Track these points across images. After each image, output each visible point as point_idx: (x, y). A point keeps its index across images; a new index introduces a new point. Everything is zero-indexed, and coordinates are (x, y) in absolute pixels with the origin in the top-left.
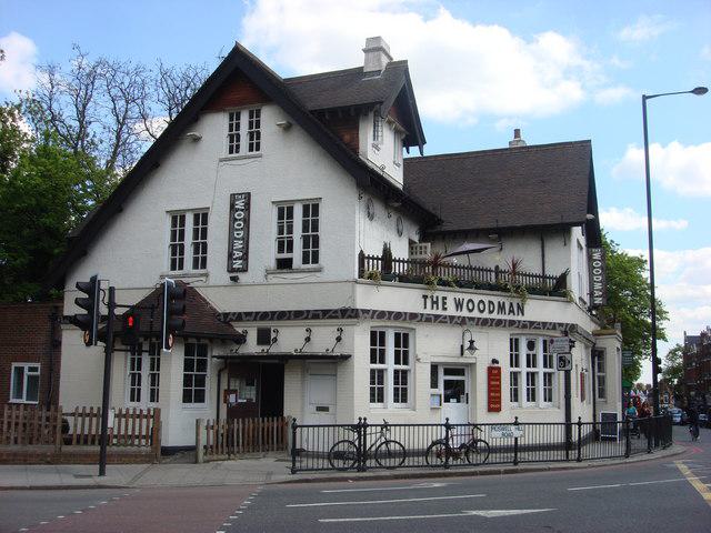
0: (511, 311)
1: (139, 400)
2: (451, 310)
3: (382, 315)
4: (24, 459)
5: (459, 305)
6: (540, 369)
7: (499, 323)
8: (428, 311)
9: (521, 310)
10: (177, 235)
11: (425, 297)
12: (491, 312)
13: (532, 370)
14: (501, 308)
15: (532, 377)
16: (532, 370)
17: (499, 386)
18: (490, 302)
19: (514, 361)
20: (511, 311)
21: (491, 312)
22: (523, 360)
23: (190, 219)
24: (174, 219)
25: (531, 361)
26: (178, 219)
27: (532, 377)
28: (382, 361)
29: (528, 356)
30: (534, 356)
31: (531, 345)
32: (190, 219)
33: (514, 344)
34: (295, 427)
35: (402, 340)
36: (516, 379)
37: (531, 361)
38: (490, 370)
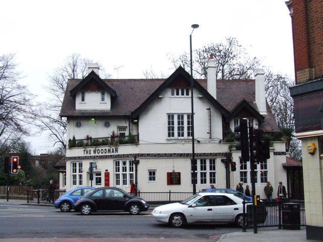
0: (113, 152)
1: (126, 184)
2: (92, 154)
3: (75, 158)
4: (217, 196)
5: (95, 152)
6: (128, 172)
7: (111, 156)
8: (85, 155)
9: (117, 151)
10: (171, 123)
11: (84, 151)
12: (105, 153)
13: (124, 173)
14: (109, 151)
15: (125, 176)
16: (124, 173)
17: (105, 181)
18: (105, 149)
19: (118, 170)
20: (113, 152)
21: (105, 153)
22: (78, 177)
23: (176, 118)
24: (169, 116)
25: (124, 169)
26: (170, 116)
27: (125, 176)
28: (126, 171)
29: (123, 167)
30: (126, 167)
31: (124, 163)
32: (176, 118)
33: (117, 164)
34: (139, 193)
35: (81, 165)
36: (80, 182)
37: (124, 169)
38: (93, 180)
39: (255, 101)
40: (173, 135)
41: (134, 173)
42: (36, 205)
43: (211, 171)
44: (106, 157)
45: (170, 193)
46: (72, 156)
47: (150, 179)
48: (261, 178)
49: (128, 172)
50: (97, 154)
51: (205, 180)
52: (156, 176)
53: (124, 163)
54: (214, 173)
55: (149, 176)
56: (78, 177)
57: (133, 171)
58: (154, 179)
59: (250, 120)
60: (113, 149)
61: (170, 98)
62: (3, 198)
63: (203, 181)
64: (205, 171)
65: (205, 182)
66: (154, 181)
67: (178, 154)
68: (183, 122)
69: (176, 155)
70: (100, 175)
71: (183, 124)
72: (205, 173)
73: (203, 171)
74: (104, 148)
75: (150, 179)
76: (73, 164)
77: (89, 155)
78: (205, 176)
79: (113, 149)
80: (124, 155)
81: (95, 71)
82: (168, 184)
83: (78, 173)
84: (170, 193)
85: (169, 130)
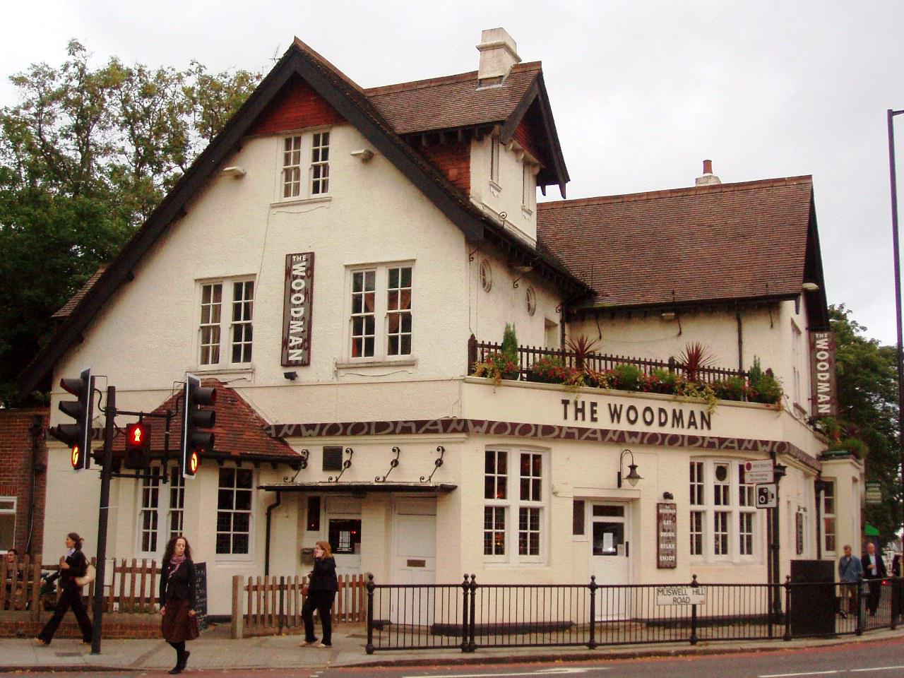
2: (604, 422)
5: (615, 414)
8: (571, 422)
9: (706, 420)
11: (566, 403)
12: (662, 424)
13: (722, 508)
15: (721, 519)
18: (661, 410)
19: (696, 495)
20: (692, 424)
21: (662, 424)
25: (721, 495)
27: (721, 519)
29: (717, 488)
30: (726, 488)
31: (721, 473)
33: (696, 471)
35: (531, 465)
37: (721, 495)
40: (370, 350)
44: (673, 441)
45: (593, 587)
46: (508, 420)
50: (624, 426)
53: (721, 473)
54: (535, 512)
60: (692, 413)
62: (16, 632)
65: (500, 551)
67: (323, 426)
68: (217, 310)
69: (637, 440)
71: (217, 318)
72: (501, 510)
74: (655, 406)
77: (587, 424)
79: (692, 413)
80: (741, 442)
83: (513, 502)
84: (593, 587)
85: (357, 330)
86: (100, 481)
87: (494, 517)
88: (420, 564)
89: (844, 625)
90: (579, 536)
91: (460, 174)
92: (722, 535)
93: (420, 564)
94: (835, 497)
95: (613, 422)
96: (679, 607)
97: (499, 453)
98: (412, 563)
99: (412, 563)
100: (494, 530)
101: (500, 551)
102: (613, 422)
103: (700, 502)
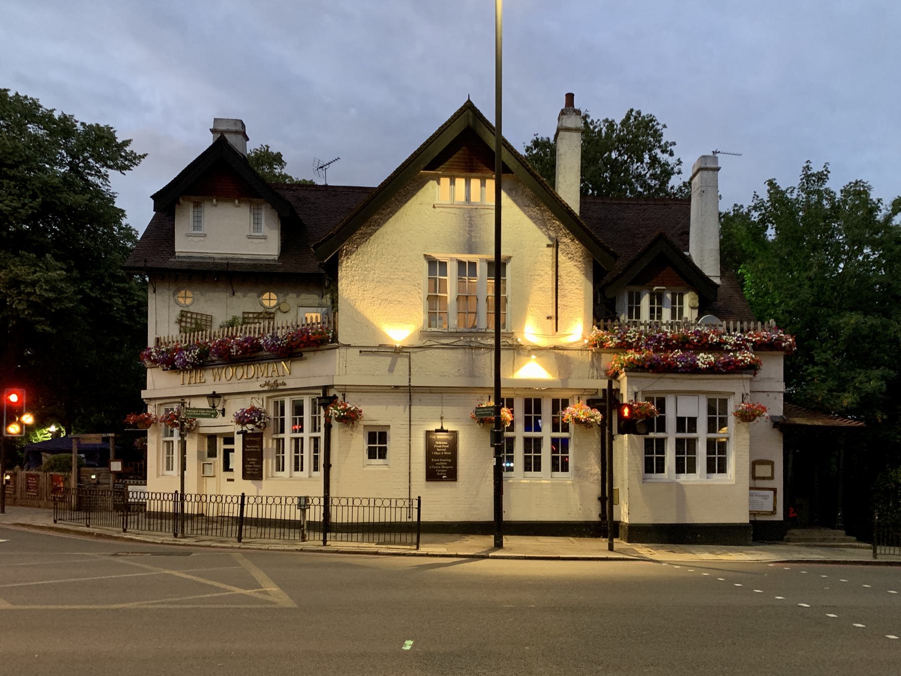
15: (299, 443)
36: (297, 463)
39: (688, 250)
41: (321, 434)
42: (867, 563)
43: (681, 435)
47: (372, 454)
48: (708, 459)
49: (307, 434)
51: (538, 460)
52: (366, 446)
55: (388, 445)
56: (289, 446)
57: (319, 430)
58: (383, 454)
59: (674, 295)
61: (188, 235)
63: (531, 465)
64: (661, 435)
65: (538, 468)
66: (381, 461)
70: (300, 432)
72: (538, 441)
73: (533, 434)
75: (372, 454)
76: (276, 403)
78: (538, 450)
81: (232, 139)
82: (427, 480)
86: (331, 463)
87: (533, 445)
88: (229, 480)
89: (56, 115)
90: (372, 460)
91: (599, 359)
92: (298, 453)
93: (229, 480)
94: (291, 417)
95: (404, 411)
96: (132, 517)
97: (380, 433)
98: (233, 480)
99: (233, 480)
100: (533, 454)
101: (538, 468)
102: (404, 411)
103: (297, 439)
